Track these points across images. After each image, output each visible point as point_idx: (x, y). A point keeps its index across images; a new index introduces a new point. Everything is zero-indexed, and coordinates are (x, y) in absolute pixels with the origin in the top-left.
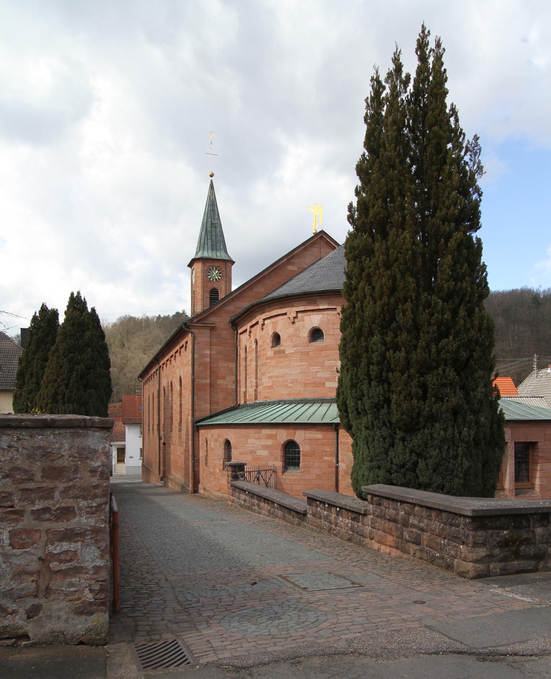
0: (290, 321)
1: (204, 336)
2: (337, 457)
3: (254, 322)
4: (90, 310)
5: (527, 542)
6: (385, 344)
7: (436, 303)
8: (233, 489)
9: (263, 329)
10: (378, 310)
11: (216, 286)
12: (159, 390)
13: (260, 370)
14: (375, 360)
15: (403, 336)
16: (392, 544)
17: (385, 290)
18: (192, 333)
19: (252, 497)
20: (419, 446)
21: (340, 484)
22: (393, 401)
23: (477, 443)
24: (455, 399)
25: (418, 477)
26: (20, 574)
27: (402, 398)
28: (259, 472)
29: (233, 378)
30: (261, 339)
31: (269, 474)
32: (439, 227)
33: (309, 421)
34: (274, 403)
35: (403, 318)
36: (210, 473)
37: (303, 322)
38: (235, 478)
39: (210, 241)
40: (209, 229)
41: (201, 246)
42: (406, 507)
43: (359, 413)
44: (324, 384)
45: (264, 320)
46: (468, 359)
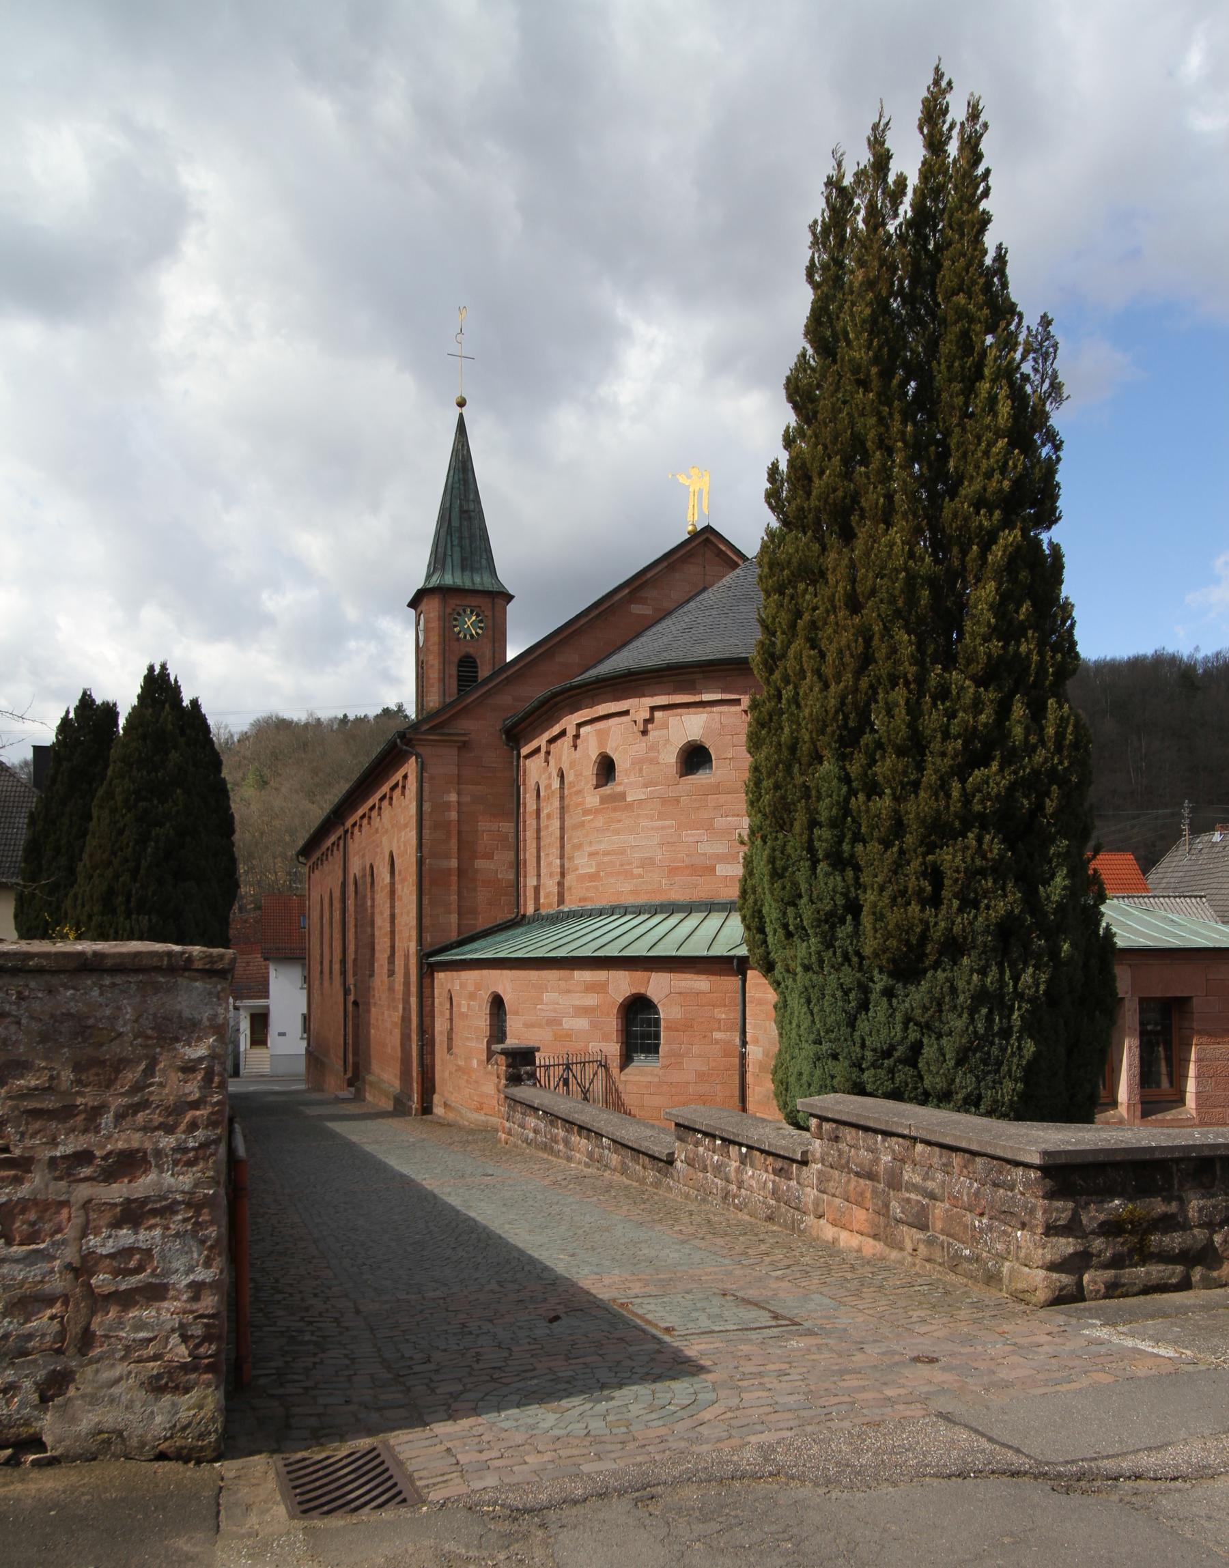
0: (635, 729)
2: (744, 1032)
3: (556, 730)
4: (186, 703)
6: (847, 779)
7: (962, 688)
8: (509, 1106)
9: (575, 747)
11: (471, 650)
12: (344, 885)
13: (570, 839)
14: (823, 817)
17: (847, 659)
19: (552, 1123)
20: (925, 1009)
21: (749, 1092)
28: (568, 1067)
29: (511, 856)
30: (571, 768)
31: (590, 1070)
34: (601, 912)
36: (459, 1069)
37: (665, 731)
38: (515, 1079)
39: (457, 549)
40: (455, 523)
41: (438, 560)
43: (789, 935)
44: (713, 869)
45: (579, 725)
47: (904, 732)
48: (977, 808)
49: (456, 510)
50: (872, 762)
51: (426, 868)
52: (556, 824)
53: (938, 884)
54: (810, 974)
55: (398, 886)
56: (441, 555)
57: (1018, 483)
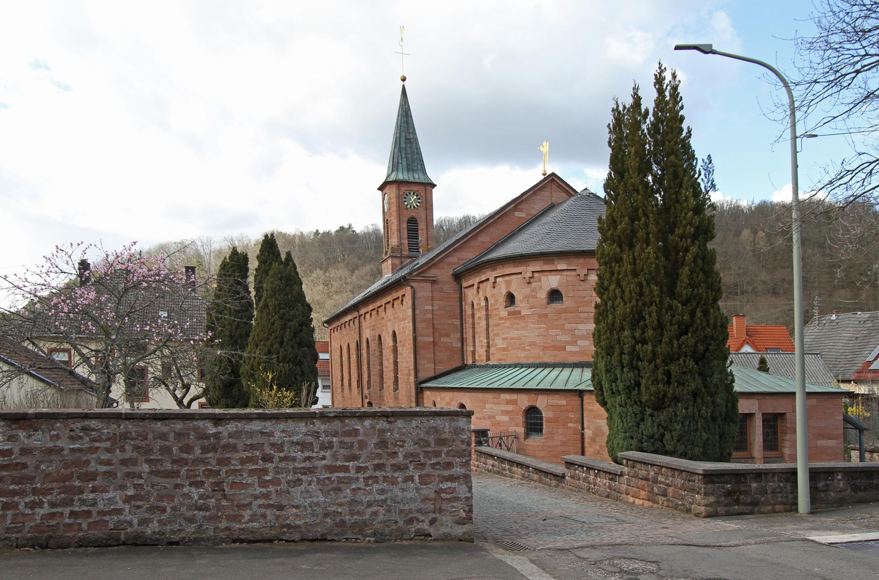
1: (424, 290)
3: (483, 278)
5: (744, 492)
6: (634, 337)
7: (677, 307)
10: (628, 310)
11: (414, 214)
14: (626, 351)
15: (650, 333)
16: (645, 497)
17: (633, 294)
18: (412, 287)
19: (502, 462)
20: (665, 421)
22: (643, 385)
23: (714, 419)
24: (695, 383)
26: (425, 499)
27: (650, 383)
28: (501, 438)
29: (459, 335)
32: (677, 243)
33: (552, 388)
35: (651, 319)
40: (403, 146)
41: (395, 166)
42: (655, 468)
43: (613, 393)
46: (705, 352)
49: (403, 139)
50: (643, 332)
55: (400, 349)
56: (395, 163)
57: (697, 228)
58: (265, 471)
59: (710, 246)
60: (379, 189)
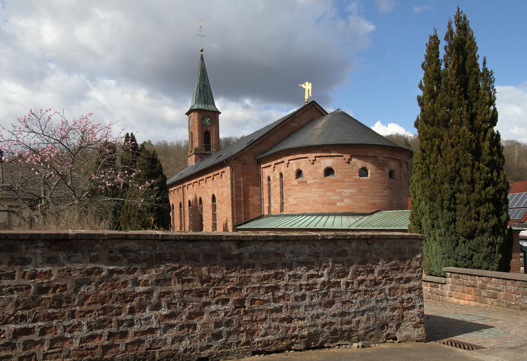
9: (288, 167)
13: (286, 193)
16: (472, 299)
25: (472, 263)
40: (202, 89)
44: (336, 204)
47: (470, 179)
48: (488, 197)
49: (202, 85)
51: (234, 200)
52: (278, 189)
53: (479, 216)
54: (441, 237)
58: (276, 288)
59: (495, 129)
60: (187, 114)
